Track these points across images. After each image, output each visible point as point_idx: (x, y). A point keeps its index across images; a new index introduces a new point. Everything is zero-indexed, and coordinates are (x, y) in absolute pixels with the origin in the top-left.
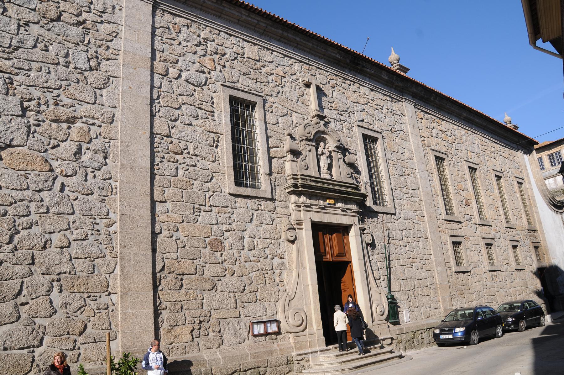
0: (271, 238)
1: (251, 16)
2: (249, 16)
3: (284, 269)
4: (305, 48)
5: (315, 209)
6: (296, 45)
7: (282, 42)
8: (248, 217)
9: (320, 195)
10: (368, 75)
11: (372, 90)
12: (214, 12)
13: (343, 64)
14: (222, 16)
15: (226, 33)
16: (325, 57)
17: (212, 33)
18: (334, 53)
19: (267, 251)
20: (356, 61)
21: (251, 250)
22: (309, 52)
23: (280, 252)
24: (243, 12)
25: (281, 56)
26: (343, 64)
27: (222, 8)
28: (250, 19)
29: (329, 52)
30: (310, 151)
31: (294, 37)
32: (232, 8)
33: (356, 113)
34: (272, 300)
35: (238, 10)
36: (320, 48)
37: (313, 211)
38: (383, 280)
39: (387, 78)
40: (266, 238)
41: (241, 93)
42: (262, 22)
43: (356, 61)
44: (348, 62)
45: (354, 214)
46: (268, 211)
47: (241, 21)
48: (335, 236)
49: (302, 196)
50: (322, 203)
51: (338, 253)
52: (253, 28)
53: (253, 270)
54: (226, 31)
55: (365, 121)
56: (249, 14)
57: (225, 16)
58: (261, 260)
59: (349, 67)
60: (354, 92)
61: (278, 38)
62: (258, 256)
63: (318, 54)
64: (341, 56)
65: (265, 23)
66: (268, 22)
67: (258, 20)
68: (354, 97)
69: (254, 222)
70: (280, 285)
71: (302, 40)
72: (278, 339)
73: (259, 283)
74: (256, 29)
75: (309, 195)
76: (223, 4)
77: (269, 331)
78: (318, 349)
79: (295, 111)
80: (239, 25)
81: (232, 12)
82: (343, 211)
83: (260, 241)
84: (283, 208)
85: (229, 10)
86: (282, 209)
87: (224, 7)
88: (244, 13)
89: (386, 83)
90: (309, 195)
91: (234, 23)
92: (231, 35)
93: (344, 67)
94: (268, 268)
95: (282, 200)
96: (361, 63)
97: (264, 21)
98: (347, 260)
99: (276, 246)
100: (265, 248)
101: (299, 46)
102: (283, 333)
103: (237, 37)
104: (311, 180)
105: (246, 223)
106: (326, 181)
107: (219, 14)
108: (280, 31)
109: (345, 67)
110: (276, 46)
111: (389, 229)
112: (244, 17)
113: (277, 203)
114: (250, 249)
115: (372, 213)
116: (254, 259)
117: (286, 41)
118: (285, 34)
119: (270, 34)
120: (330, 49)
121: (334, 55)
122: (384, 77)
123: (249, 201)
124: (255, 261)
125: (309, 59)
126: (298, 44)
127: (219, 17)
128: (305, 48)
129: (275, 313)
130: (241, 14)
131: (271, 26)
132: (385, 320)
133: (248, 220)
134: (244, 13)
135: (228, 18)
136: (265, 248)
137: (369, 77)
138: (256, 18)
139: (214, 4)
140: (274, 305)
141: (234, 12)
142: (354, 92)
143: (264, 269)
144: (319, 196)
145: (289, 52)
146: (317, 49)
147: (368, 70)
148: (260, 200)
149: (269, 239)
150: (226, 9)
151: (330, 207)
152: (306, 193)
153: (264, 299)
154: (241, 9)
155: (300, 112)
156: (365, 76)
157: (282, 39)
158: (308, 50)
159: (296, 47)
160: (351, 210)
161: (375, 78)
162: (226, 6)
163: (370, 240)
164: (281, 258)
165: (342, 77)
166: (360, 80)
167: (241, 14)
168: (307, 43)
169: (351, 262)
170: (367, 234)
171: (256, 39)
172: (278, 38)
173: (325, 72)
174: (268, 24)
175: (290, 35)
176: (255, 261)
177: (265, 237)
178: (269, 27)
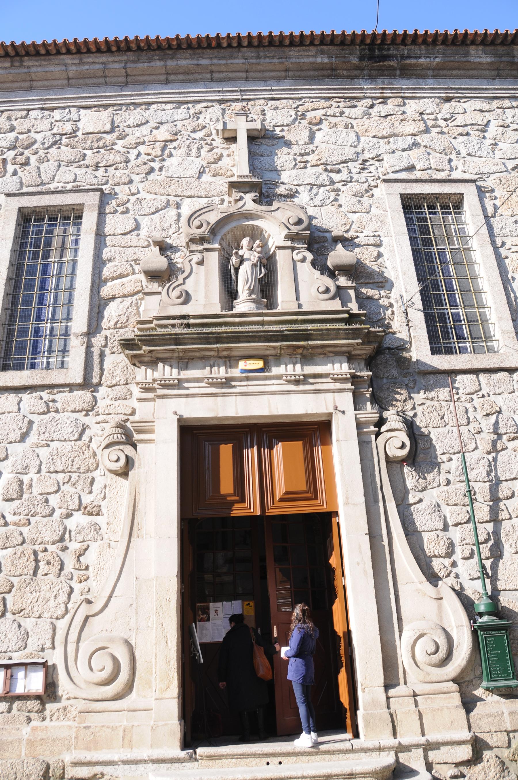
0: (69, 469)
1: (85, 60)
2: (81, 63)
3: (95, 539)
4: (232, 75)
5: (194, 388)
6: (208, 76)
7: (174, 82)
8: (17, 431)
9: (212, 353)
10: (430, 72)
11: (448, 100)
12: (17, 85)
13: (345, 73)
14: (35, 84)
15: (42, 109)
16: (290, 74)
17: (13, 118)
18: (308, 56)
19: (54, 501)
20: (377, 52)
21: (12, 500)
22: (247, 79)
23: (89, 501)
24: (68, 59)
25: (169, 106)
26: (345, 73)
27: (26, 70)
28: (86, 67)
29: (293, 60)
30: (201, 263)
31: (195, 62)
32: (45, 63)
33: (385, 157)
34: (46, 615)
35: (56, 62)
36: (267, 60)
37: (187, 396)
38: (466, 559)
39: (489, 60)
40: (56, 472)
41: (47, 197)
42: (113, 62)
43: (377, 52)
44: (355, 60)
45: (338, 386)
46: (72, 412)
47: (73, 78)
48: (279, 449)
49: (160, 365)
50: (221, 372)
51: (284, 491)
52: (102, 80)
53: (7, 545)
54: (40, 106)
55: (418, 168)
56: (81, 60)
57: (40, 83)
58: (33, 520)
59: (366, 72)
60: (386, 116)
61: (163, 77)
62: (25, 512)
63: (268, 74)
64: (330, 57)
65: (121, 62)
66: (125, 58)
67: (103, 63)
68: (385, 128)
69: (32, 438)
70: (75, 578)
71: (215, 61)
72: (47, 713)
73: (18, 573)
74: (108, 80)
75: (180, 359)
76: (25, 64)
77: (19, 689)
78: (144, 754)
79: (188, 194)
80: (73, 86)
81: (47, 69)
82: (297, 382)
83: (39, 479)
84: (116, 399)
85: (39, 69)
86: (113, 402)
87: (28, 67)
88: (70, 61)
89: (494, 73)
90: (180, 359)
91: (62, 87)
92: (52, 109)
93: (352, 78)
94: (47, 539)
95: (114, 382)
96: (392, 52)
97: (117, 59)
98: (325, 508)
99: (79, 488)
100: (48, 494)
101: (216, 75)
102: (64, 697)
103: (64, 108)
104: (188, 325)
105: (11, 443)
106: (237, 320)
107: (27, 84)
108: (159, 64)
109: (356, 77)
110: (154, 94)
111: (500, 412)
112: (74, 68)
113: (103, 391)
114: (9, 497)
115: (430, 377)
116: (16, 518)
117: (181, 77)
118: (171, 64)
119: (141, 78)
120: (291, 53)
121: (311, 60)
122: (478, 60)
123: (26, 397)
124: (15, 524)
125: (241, 90)
126: (212, 72)
127: (31, 88)
128: (232, 75)
129: (48, 644)
130: (66, 65)
131: (134, 62)
132: (454, 680)
133: (16, 435)
134: (70, 61)
135: (46, 83)
136: (48, 494)
137: (435, 77)
138: (97, 60)
139: (9, 71)
140: (49, 627)
141: (52, 68)
142: (386, 116)
143: (39, 541)
144: (211, 357)
145: (189, 93)
146: (259, 64)
147: (421, 60)
148: (56, 391)
149: (63, 471)
150: (34, 69)
151: (248, 379)
152: (168, 355)
153: (26, 612)
154: (62, 57)
155: (203, 194)
156: (424, 77)
157: (172, 77)
158: (243, 75)
159: (212, 80)
160: (327, 375)
161: (455, 72)
162: (30, 63)
163: (403, 446)
164: (90, 514)
165: (346, 98)
166: (402, 89)
167: (66, 65)
168: (229, 62)
169: (336, 514)
170: (389, 434)
171: (106, 97)
172: (163, 77)
173: (291, 102)
174: (126, 62)
175: (183, 62)
176: (15, 524)
177: (52, 469)
178: (130, 65)
